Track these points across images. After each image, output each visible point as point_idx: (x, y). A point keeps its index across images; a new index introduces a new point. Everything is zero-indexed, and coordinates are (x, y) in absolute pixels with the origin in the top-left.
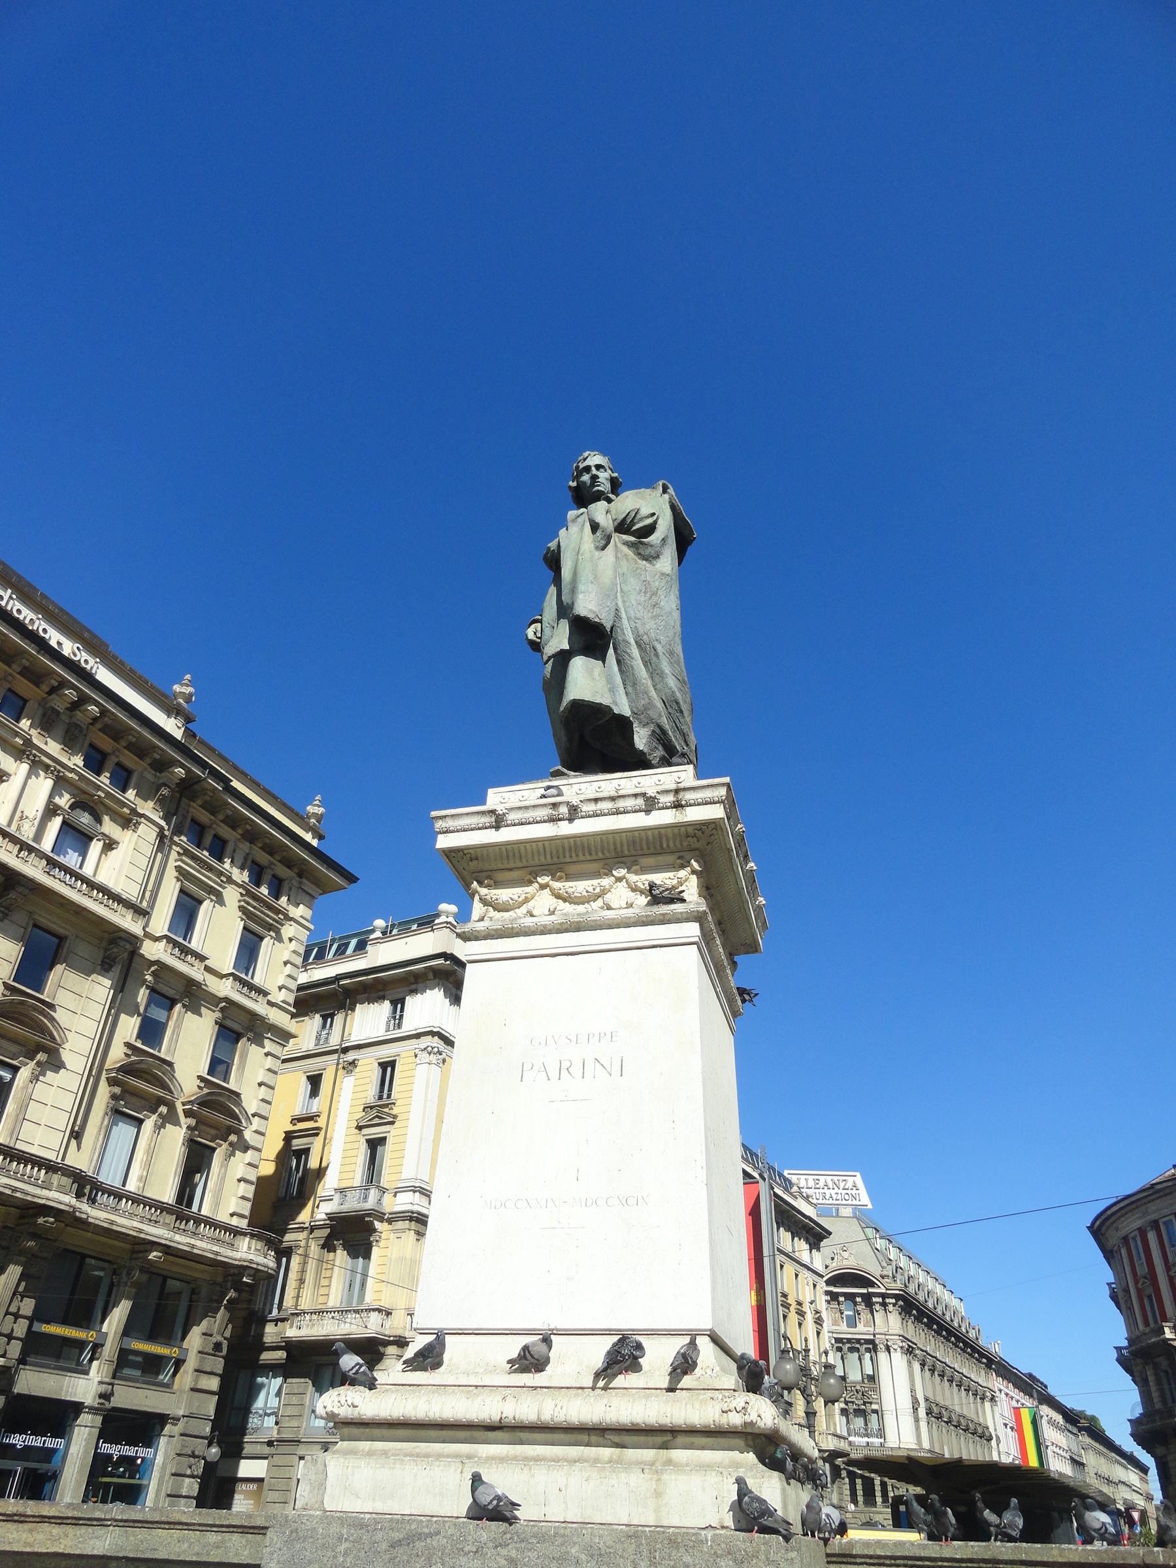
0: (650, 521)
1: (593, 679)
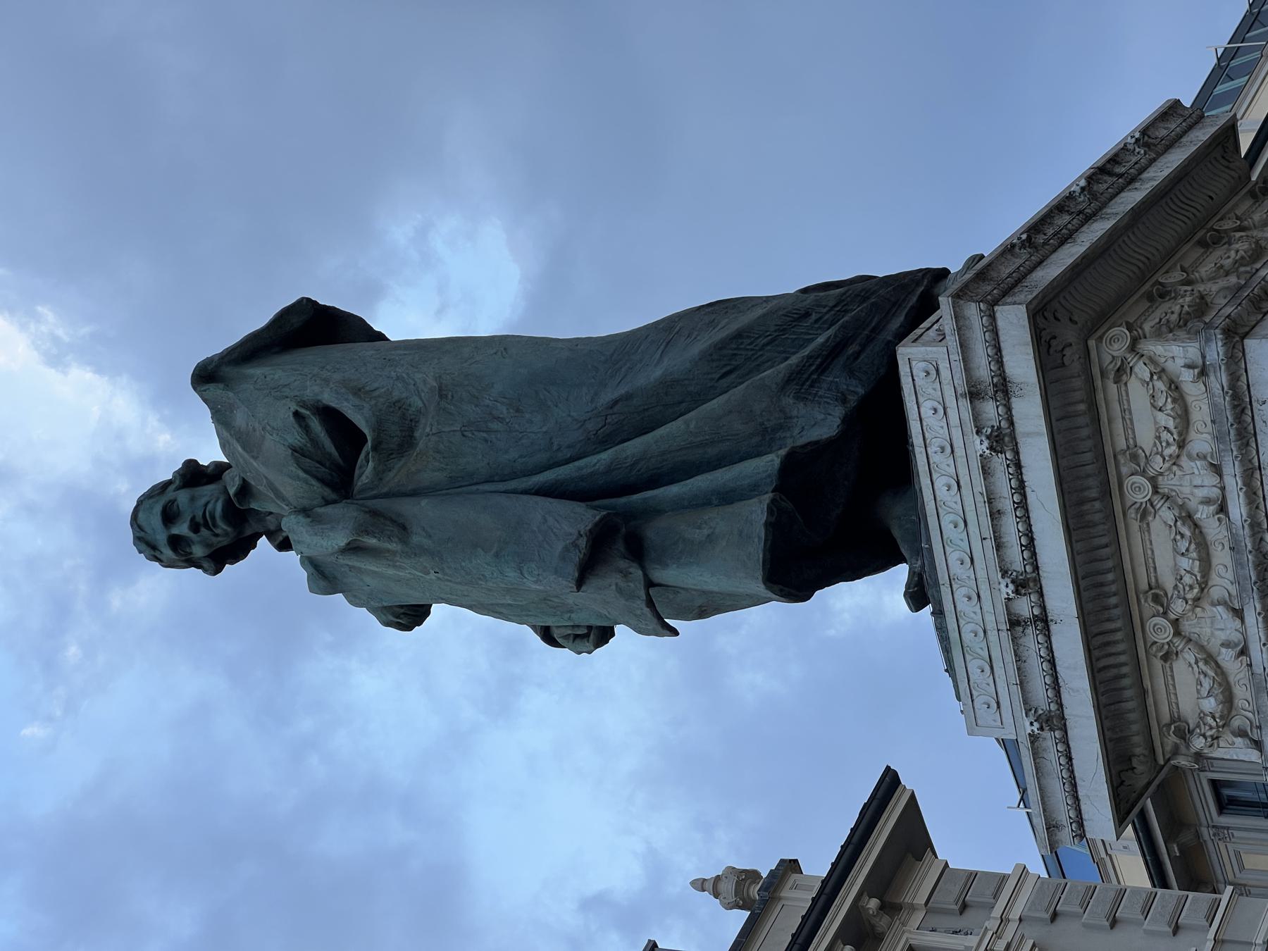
0: (316, 425)
1: (711, 539)
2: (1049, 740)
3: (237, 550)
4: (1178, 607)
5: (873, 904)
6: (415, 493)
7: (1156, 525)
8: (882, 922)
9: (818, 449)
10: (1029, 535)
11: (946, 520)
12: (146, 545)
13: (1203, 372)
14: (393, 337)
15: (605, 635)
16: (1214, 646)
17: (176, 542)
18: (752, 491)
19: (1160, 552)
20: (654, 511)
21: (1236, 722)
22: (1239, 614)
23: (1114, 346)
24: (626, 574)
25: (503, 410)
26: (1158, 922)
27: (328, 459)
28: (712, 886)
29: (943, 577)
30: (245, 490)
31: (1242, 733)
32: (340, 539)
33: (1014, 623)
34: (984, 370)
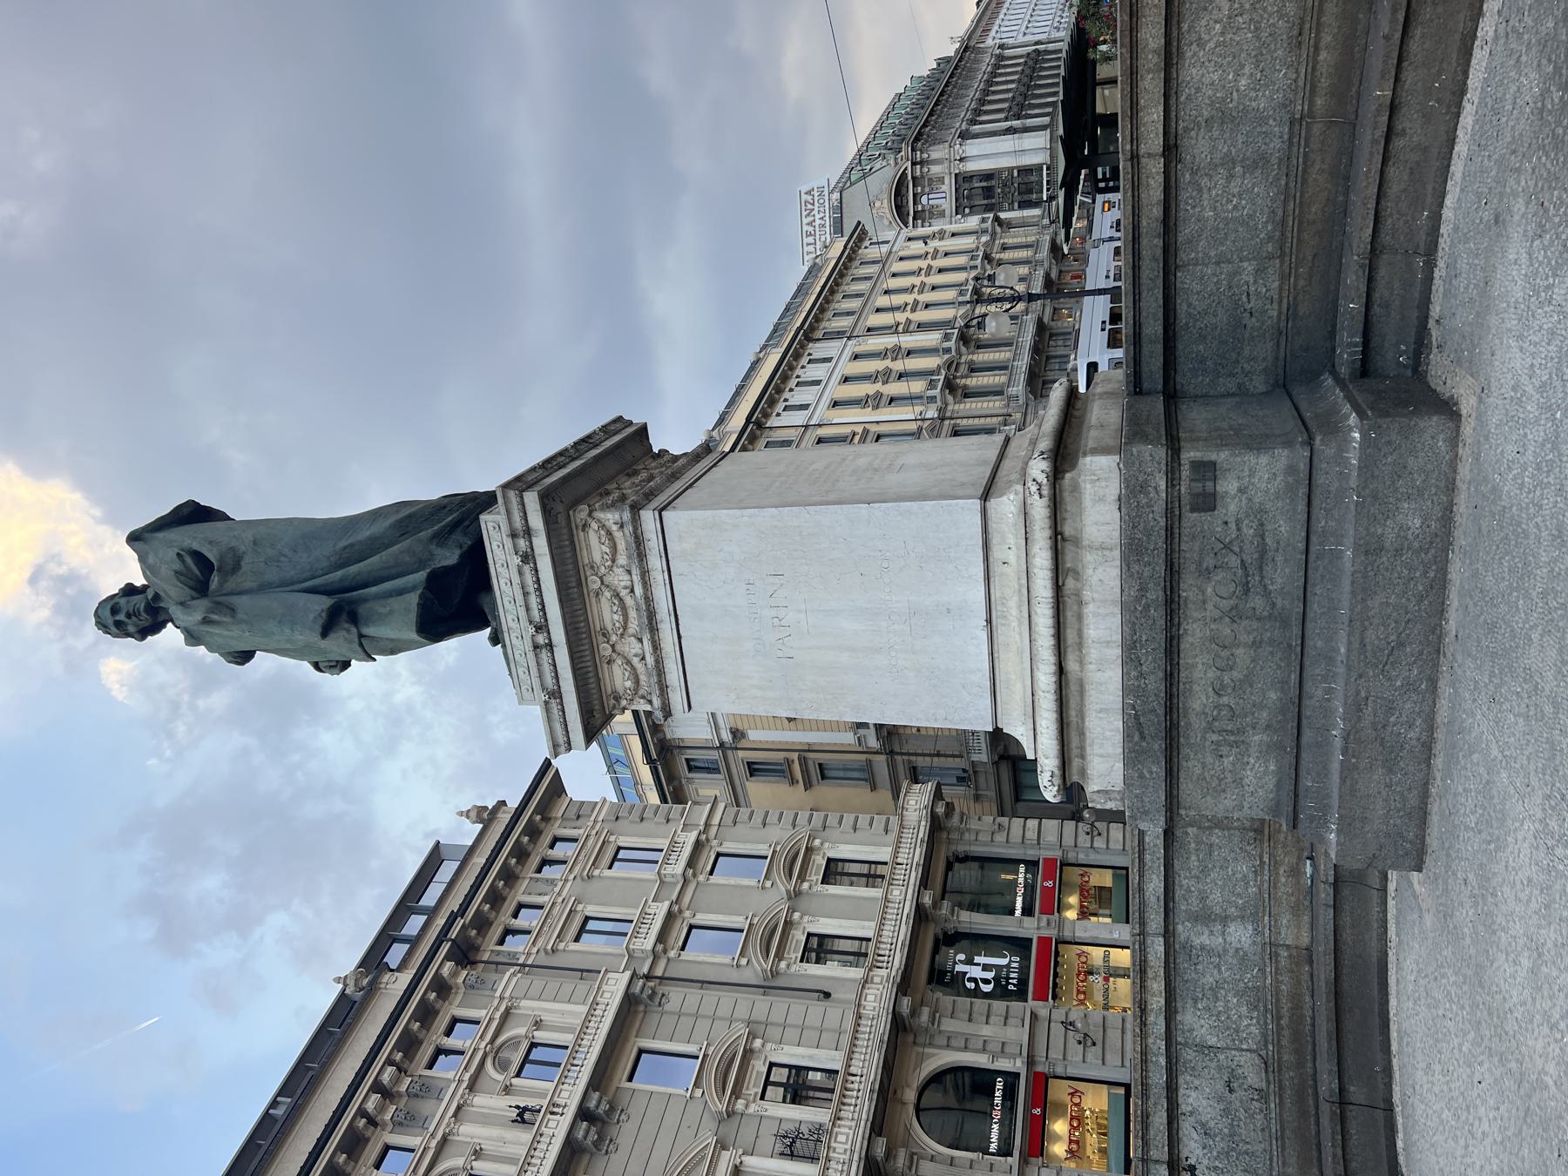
0: (189, 560)
1: (391, 612)
2: (554, 704)
3: (156, 628)
4: (614, 638)
5: (538, 818)
6: (241, 593)
7: (603, 600)
8: (542, 825)
9: (447, 570)
10: (542, 604)
11: (506, 600)
12: (101, 625)
13: (622, 526)
14: (237, 515)
15: (345, 665)
16: (630, 656)
17: (118, 624)
18: (414, 588)
19: (605, 613)
20: (364, 600)
21: (641, 692)
22: (640, 640)
23: (582, 513)
24: (348, 631)
25: (286, 551)
26: (660, 818)
27: (198, 577)
28: (467, 814)
29: (505, 628)
30: (157, 597)
31: (643, 697)
32: (198, 617)
33: (536, 647)
34: (518, 523)
